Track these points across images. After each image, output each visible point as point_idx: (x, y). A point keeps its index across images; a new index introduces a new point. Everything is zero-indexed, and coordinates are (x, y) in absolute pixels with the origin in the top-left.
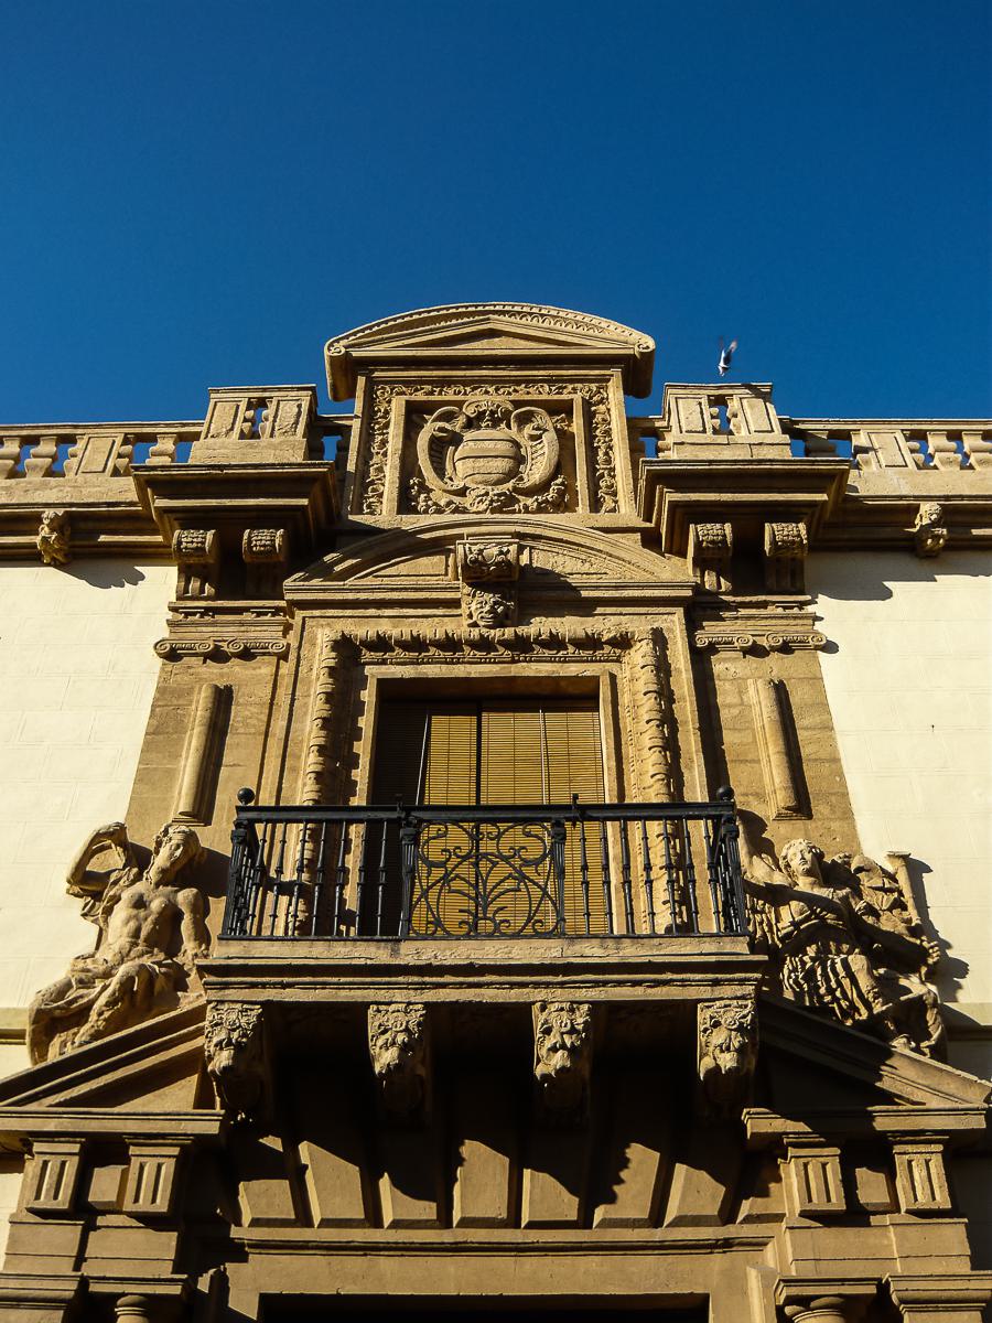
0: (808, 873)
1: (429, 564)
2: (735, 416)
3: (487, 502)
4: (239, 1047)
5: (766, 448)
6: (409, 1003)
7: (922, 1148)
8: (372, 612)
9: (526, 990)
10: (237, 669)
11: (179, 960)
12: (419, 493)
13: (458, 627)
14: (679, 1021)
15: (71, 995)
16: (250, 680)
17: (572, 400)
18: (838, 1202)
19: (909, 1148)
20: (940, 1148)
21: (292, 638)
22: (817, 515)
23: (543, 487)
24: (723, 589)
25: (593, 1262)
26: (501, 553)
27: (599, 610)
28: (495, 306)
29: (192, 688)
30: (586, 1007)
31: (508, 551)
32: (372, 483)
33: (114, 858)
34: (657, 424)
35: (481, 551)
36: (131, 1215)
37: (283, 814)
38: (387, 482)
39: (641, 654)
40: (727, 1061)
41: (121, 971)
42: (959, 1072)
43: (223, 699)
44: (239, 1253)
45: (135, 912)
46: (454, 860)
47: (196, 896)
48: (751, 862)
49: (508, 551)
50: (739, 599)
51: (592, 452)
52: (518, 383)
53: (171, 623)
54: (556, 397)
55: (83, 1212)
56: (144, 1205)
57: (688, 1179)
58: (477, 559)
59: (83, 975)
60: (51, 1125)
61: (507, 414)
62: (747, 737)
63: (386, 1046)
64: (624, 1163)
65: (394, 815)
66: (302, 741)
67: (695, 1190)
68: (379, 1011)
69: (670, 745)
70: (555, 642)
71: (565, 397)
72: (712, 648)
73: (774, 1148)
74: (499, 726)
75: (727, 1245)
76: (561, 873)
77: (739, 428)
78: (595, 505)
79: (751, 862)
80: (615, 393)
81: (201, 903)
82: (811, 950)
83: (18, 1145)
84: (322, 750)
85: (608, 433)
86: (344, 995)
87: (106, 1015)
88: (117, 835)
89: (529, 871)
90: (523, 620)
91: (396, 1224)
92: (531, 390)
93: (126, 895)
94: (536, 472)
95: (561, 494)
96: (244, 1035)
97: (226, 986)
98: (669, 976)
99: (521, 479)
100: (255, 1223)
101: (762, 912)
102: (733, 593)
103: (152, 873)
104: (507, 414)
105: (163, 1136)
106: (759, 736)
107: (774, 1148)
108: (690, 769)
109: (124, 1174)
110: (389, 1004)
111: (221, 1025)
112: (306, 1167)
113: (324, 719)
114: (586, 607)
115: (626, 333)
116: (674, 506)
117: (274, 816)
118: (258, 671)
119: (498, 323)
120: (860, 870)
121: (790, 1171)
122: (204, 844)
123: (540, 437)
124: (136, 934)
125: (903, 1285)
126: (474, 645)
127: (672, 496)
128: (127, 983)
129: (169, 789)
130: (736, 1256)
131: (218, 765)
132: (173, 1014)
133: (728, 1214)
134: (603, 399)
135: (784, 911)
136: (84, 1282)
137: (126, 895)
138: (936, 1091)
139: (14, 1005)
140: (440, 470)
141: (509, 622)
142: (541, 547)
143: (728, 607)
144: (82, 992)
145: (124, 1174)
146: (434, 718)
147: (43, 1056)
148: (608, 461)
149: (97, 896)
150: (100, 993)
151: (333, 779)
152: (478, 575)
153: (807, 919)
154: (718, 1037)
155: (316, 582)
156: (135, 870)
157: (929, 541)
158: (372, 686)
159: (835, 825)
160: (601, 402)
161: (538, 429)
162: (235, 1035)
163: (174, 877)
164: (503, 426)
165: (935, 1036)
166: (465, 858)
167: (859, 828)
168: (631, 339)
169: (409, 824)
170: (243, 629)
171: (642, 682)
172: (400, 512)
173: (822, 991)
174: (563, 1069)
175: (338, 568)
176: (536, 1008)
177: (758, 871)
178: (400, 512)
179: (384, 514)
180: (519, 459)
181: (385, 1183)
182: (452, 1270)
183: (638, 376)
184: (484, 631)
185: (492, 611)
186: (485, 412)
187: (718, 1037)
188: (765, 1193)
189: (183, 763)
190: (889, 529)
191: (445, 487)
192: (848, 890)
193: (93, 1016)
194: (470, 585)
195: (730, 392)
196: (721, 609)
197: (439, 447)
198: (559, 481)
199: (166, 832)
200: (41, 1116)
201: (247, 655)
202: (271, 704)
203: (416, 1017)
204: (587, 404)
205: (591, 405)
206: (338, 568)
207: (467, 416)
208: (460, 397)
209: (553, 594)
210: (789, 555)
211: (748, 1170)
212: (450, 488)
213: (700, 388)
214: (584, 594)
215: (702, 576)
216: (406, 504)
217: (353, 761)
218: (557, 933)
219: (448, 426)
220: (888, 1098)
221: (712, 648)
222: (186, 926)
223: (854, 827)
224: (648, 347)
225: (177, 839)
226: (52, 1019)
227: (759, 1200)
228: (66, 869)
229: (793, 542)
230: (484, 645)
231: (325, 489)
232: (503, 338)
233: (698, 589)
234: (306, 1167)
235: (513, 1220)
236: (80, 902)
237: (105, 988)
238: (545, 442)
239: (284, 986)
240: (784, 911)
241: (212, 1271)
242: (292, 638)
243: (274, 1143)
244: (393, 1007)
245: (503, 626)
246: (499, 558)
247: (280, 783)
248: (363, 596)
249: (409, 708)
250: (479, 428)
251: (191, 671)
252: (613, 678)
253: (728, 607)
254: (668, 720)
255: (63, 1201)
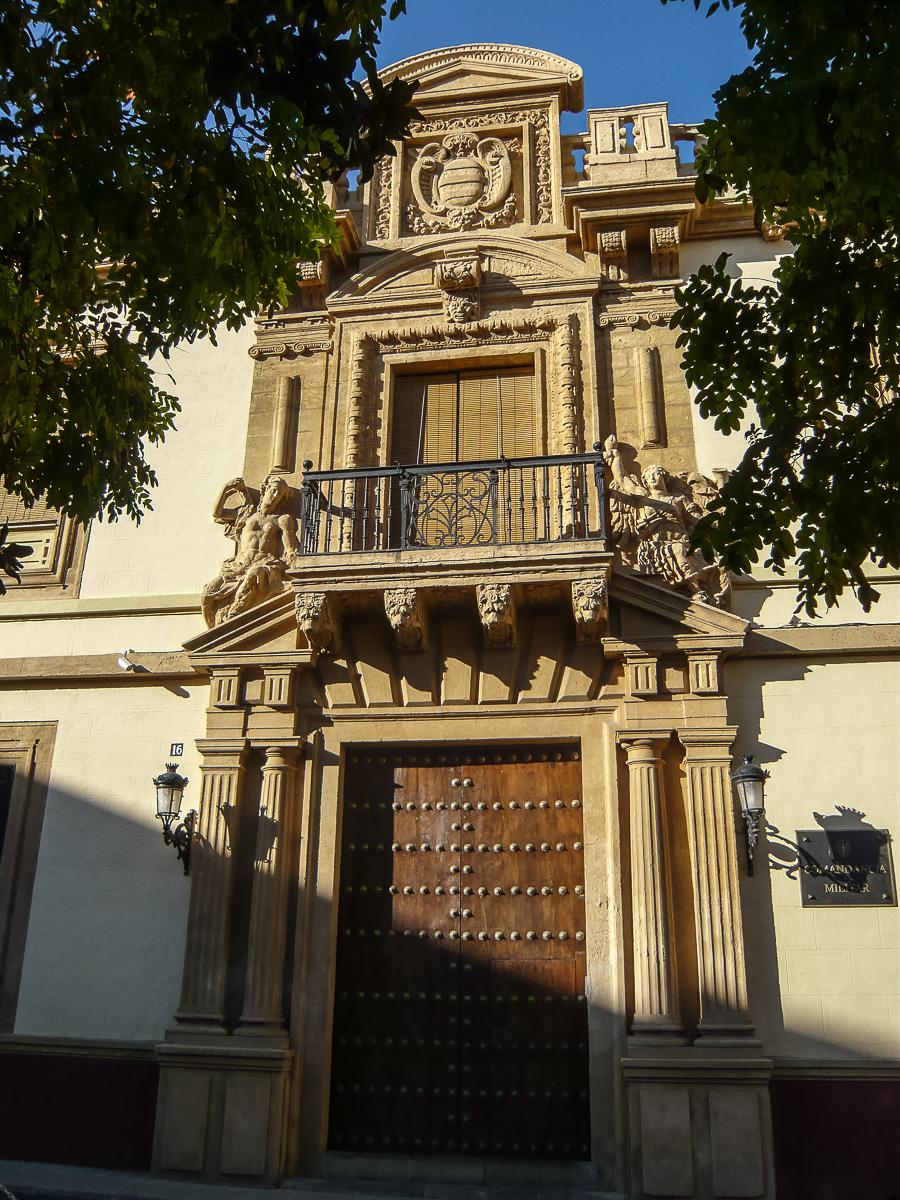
0: (657, 488)
1: (421, 276)
2: (638, 134)
3: (461, 221)
4: (314, 618)
5: (657, 162)
6: (407, 589)
7: (705, 657)
8: (385, 315)
9: (472, 578)
10: (302, 363)
11: (283, 559)
12: (414, 216)
13: (440, 323)
14: (561, 595)
15: (224, 586)
16: (310, 370)
17: (521, 127)
18: (653, 689)
19: (697, 658)
20: (716, 657)
21: (335, 337)
22: (689, 218)
23: (500, 205)
24: (622, 279)
25: (517, 721)
26: (466, 269)
27: (535, 303)
28: (464, 48)
29: (275, 380)
30: (507, 586)
31: (471, 267)
32: (382, 212)
33: (239, 499)
34: (585, 140)
35: (452, 269)
36: (267, 706)
37: (333, 474)
38: (392, 209)
39: (561, 335)
40: (587, 615)
41: (249, 572)
42: (729, 614)
43: (295, 385)
44: (328, 722)
45: (254, 532)
46: (432, 499)
47: (288, 519)
48: (622, 481)
49: (471, 267)
50: (632, 285)
51: (535, 169)
52: (483, 114)
53: (257, 333)
54: (510, 125)
55: (244, 705)
56: (275, 701)
57: (571, 676)
58: (449, 277)
59: (229, 574)
60: (221, 662)
61: (475, 144)
62: (628, 391)
63: (394, 614)
64: (537, 667)
65: (395, 472)
66: (345, 413)
67: (575, 681)
68: (390, 594)
69: (577, 402)
70: (505, 330)
71: (516, 125)
72: (611, 326)
73: (619, 660)
74: (471, 389)
75: (592, 711)
76: (495, 504)
77: (640, 146)
78: (535, 220)
79: (622, 481)
80: (553, 117)
81: (292, 523)
82: (656, 537)
83: (205, 672)
84: (357, 419)
85: (547, 153)
86: (370, 586)
87: (244, 598)
88: (238, 485)
89: (476, 503)
90: (484, 315)
91: (410, 705)
92: (493, 119)
93: (249, 522)
94: (495, 192)
95: (512, 209)
96: (317, 611)
97: (304, 584)
98: (555, 566)
99: (485, 198)
100: (335, 706)
101: (629, 512)
102: (630, 281)
103: (262, 507)
104: (475, 144)
105: (282, 664)
106: (638, 391)
107: (619, 660)
108: (589, 417)
109: (263, 684)
110: (396, 589)
111: (306, 603)
112: (360, 675)
113: (357, 398)
114: (526, 302)
115: (562, 64)
116: (586, 221)
117: (331, 476)
118: (315, 364)
119: (468, 63)
120: (693, 482)
121: (628, 670)
122: (291, 485)
123: (497, 163)
124: (256, 546)
125: (685, 734)
126: (452, 336)
127: (585, 214)
128: (253, 579)
129: (267, 450)
130: (597, 717)
131: (296, 432)
132: (282, 595)
133: (593, 694)
134: (544, 123)
135: (641, 510)
136: (248, 742)
137: (249, 522)
138: (715, 625)
139: (193, 592)
140: (428, 198)
141: (474, 318)
142: (497, 256)
143: (625, 292)
144: (229, 584)
145: (263, 684)
146: (430, 387)
147: (213, 621)
148: (546, 178)
149: (232, 523)
150: (239, 585)
151: (365, 441)
152: (451, 286)
153: (654, 517)
154: (582, 602)
155: (346, 297)
156: (252, 506)
157: (771, 232)
158: (387, 368)
159: (682, 451)
160: (543, 125)
161: (496, 156)
162: (311, 612)
163: (276, 508)
164: (472, 154)
165: (724, 590)
166: (438, 497)
167: (696, 452)
168: (565, 69)
169: (404, 477)
170: (303, 333)
171: (560, 356)
172: (401, 235)
173: (657, 565)
174: (493, 622)
175: (361, 285)
176: (478, 588)
177: (628, 487)
178: (401, 235)
179: (390, 239)
180: (483, 182)
181: (404, 682)
182: (442, 727)
183: (571, 98)
184: (458, 324)
185: (463, 311)
186: (458, 144)
187: (582, 602)
188: (615, 683)
189: (274, 432)
190: (743, 222)
191: (432, 210)
192: (683, 496)
193: (237, 597)
194: (448, 292)
195: (636, 112)
196: (619, 294)
197: (427, 177)
198: (510, 199)
199: (267, 482)
200: (214, 657)
201: (307, 353)
202: (325, 387)
203: (411, 596)
204: (533, 128)
205: (535, 129)
206: (361, 285)
207: (447, 149)
208: (441, 132)
209: (503, 294)
210: (667, 251)
211: (606, 670)
212: (435, 211)
213: (613, 111)
214: (525, 292)
215: (608, 270)
216: (405, 230)
217: (377, 424)
218: (492, 542)
219: (432, 159)
220: (688, 630)
221: (611, 326)
222: (285, 538)
223: (694, 452)
224: (577, 76)
225: (274, 486)
226: (215, 601)
227: (611, 686)
228: (212, 510)
229: (669, 243)
230: (458, 335)
231: (347, 229)
232: (472, 76)
233: (604, 280)
234: (360, 675)
235: (474, 700)
236: (223, 527)
237: (241, 582)
238: (501, 167)
239: (337, 582)
240: (641, 510)
241: (314, 732)
242: (335, 337)
243: (342, 663)
244: (397, 591)
245: (470, 320)
246: (465, 274)
247: (333, 443)
248: (378, 305)
249: (413, 381)
250: (455, 157)
251: (273, 367)
252: (543, 352)
253: (625, 292)
254: (576, 384)
255: (232, 701)
